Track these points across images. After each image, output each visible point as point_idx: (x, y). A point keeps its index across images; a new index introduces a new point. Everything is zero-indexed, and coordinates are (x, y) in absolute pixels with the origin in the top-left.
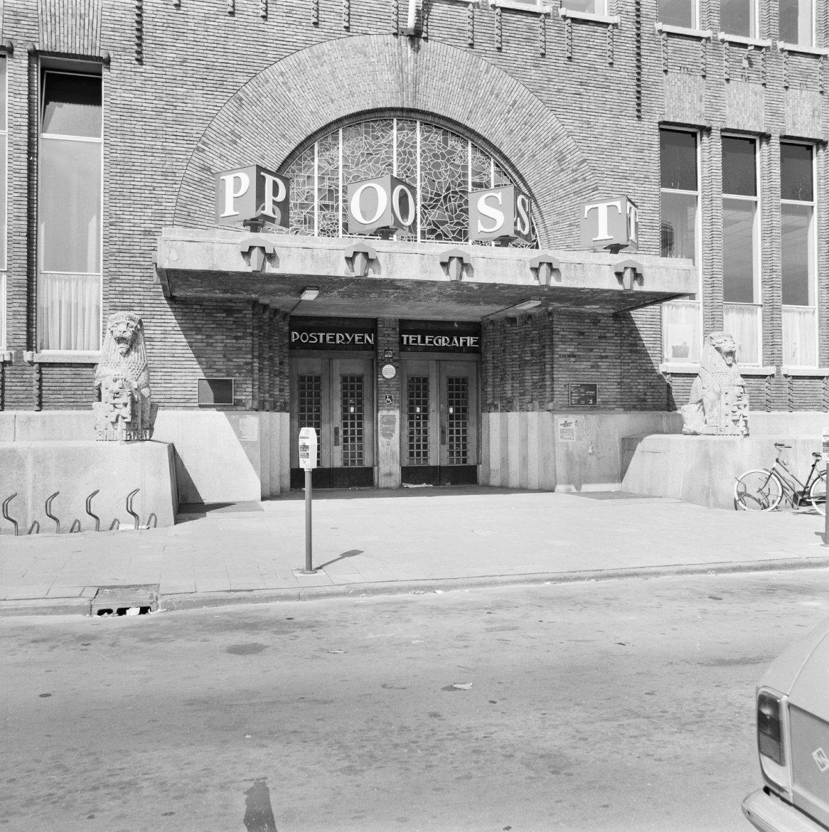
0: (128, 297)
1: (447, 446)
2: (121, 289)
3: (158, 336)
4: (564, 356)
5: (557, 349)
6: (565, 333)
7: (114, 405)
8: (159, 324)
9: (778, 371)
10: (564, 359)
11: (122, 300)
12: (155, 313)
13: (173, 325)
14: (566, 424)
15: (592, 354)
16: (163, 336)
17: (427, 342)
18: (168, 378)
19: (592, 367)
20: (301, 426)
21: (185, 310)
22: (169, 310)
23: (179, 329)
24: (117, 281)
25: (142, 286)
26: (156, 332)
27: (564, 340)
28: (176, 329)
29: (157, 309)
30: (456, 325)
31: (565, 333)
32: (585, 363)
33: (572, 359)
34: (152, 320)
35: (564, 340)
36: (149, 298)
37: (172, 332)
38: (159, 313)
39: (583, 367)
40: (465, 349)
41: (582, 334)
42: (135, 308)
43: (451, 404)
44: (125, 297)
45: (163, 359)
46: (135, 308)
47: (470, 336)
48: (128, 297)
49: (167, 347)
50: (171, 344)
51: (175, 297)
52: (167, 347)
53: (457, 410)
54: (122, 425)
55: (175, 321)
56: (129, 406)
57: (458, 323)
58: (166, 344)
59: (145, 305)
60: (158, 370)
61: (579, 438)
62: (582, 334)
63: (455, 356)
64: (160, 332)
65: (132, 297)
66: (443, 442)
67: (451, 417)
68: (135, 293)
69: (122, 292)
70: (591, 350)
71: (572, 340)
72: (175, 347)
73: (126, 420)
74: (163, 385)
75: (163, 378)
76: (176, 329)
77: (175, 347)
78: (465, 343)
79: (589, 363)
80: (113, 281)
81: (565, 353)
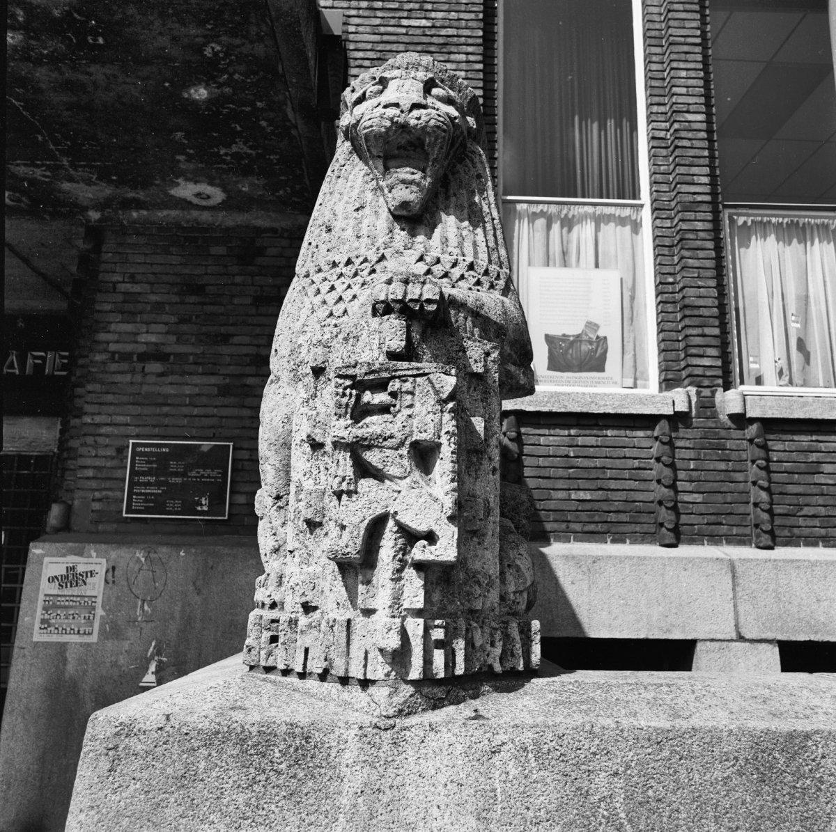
4: (125, 357)
5: (102, 336)
6: (137, 288)
7: (356, 449)
9: (707, 406)
10: (125, 366)
14: (72, 578)
15: (225, 350)
19: (224, 391)
27: (130, 307)
31: (137, 288)
32: (197, 380)
33: (155, 367)
35: (130, 307)
39: (188, 390)
41: (199, 290)
54: (395, 592)
56: (444, 465)
61: (113, 631)
62: (199, 290)
70: (225, 339)
71: (158, 307)
79: (213, 380)
81: (129, 348)
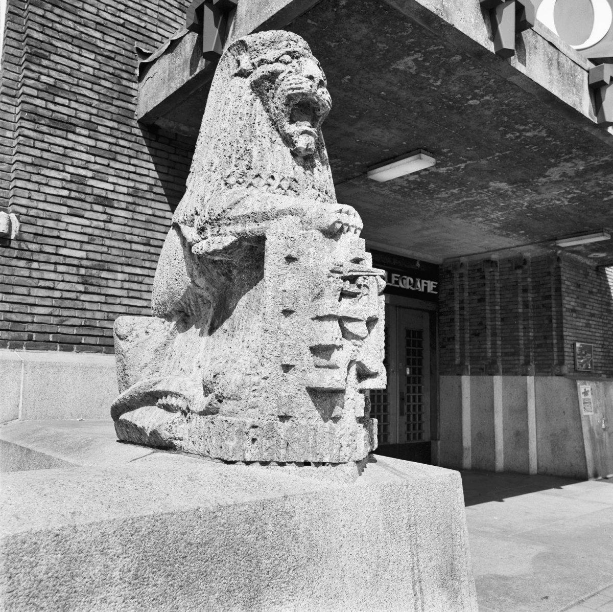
0: (66, 102)
1: (405, 417)
2: (51, 81)
3: (121, 197)
8: (124, 174)
11: (51, 106)
12: (118, 149)
13: (152, 182)
16: (130, 199)
17: (393, 282)
18: (135, 286)
20: (385, 391)
21: (173, 157)
22: (146, 150)
23: (161, 191)
24: (45, 62)
25: (96, 88)
26: (119, 189)
28: (155, 189)
29: (122, 142)
30: (418, 265)
34: (112, 164)
36: (108, 116)
37: (149, 195)
38: (126, 151)
40: (424, 295)
42: (78, 130)
43: (408, 363)
44: (58, 100)
45: (127, 246)
46: (78, 130)
47: (431, 280)
48: (66, 102)
49: (138, 224)
50: (143, 218)
51: (158, 128)
52: (138, 224)
53: (413, 371)
55: (155, 174)
57: (422, 263)
58: (137, 216)
59: (100, 129)
60: (119, 268)
63: (416, 303)
64: (125, 190)
65: (73, 104)
66: (402, 414)
67: (408, 378)
68: (81, 99)
69: (53, 90)
72: (151, 226)
73: (369, 384)
74: (126, 301)
75: (126, 285)
76: (155, 189)
77: (151, 226)
78: (426, 288)
80: (35, 60)
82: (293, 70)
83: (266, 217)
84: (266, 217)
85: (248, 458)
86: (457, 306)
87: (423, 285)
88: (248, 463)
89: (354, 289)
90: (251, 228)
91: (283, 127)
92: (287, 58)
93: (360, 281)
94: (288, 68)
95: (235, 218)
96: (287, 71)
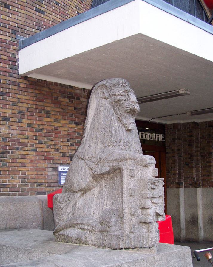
78: (158, 138)
82: (126, 99)
83: (121, 160)
84: (121, 160)
85: (121, 247)
86: (176, 148)
87: (157, 137)
88: (121, 249)
89: (155, 187)
90: (116, 164)
91: (122, 121)
92: (123, 93)
93: (156, 184)
94: (124, 98)
95: (110, 161)
96: (124, 100)
